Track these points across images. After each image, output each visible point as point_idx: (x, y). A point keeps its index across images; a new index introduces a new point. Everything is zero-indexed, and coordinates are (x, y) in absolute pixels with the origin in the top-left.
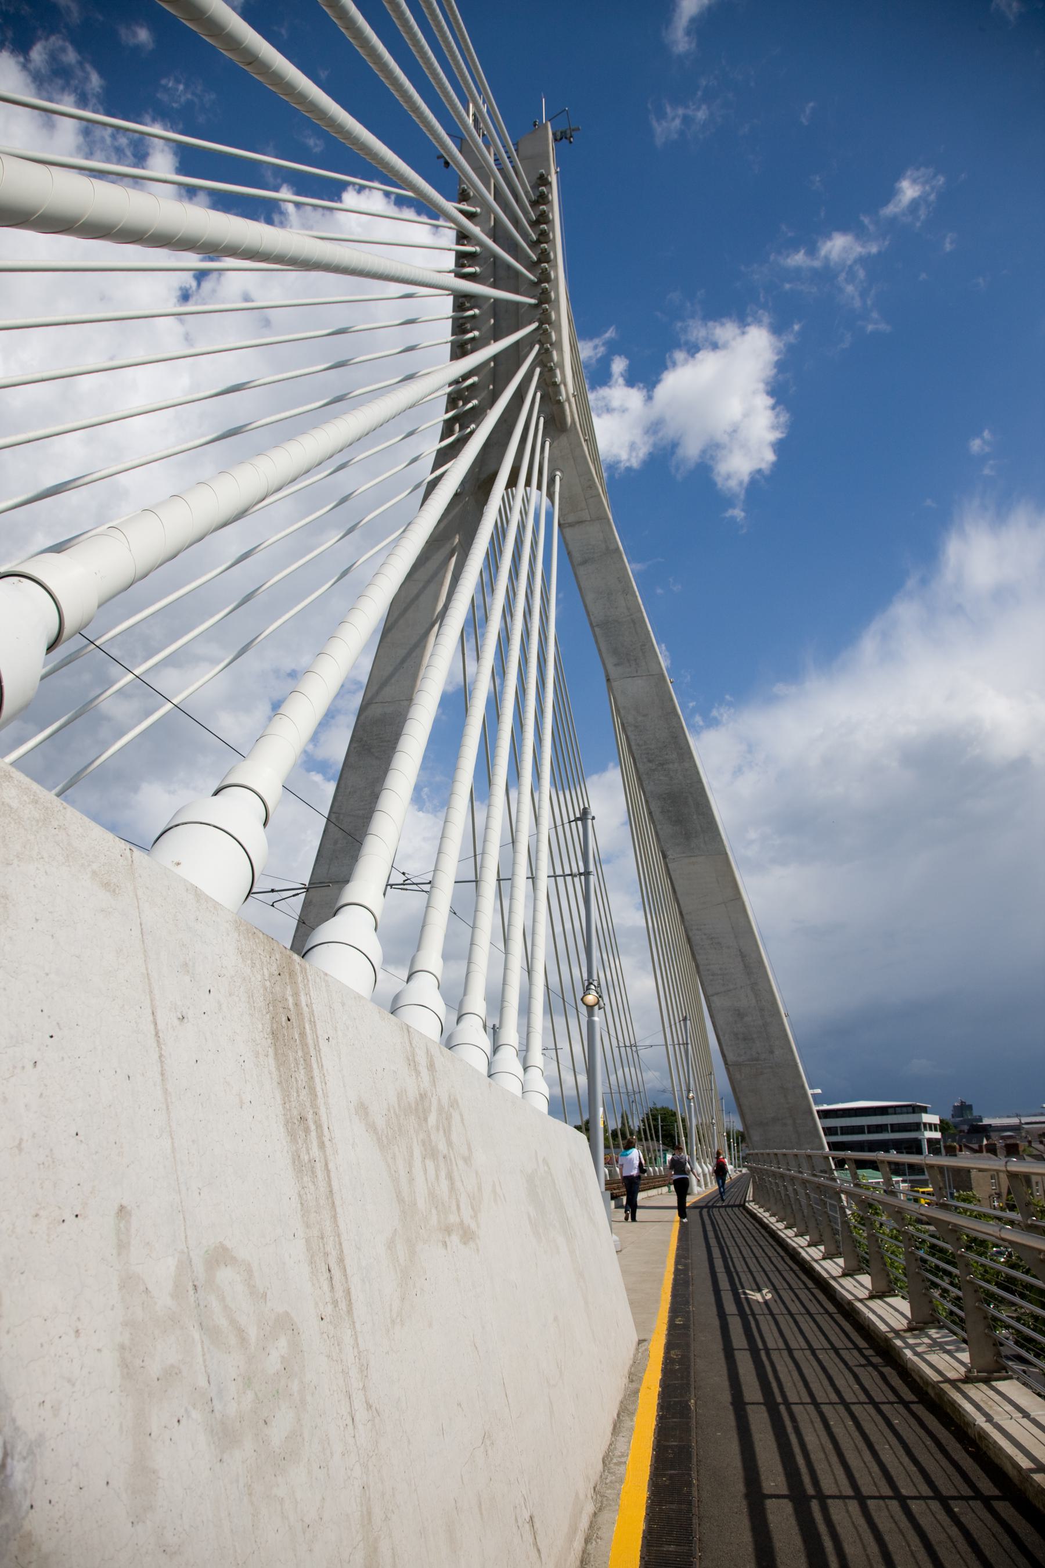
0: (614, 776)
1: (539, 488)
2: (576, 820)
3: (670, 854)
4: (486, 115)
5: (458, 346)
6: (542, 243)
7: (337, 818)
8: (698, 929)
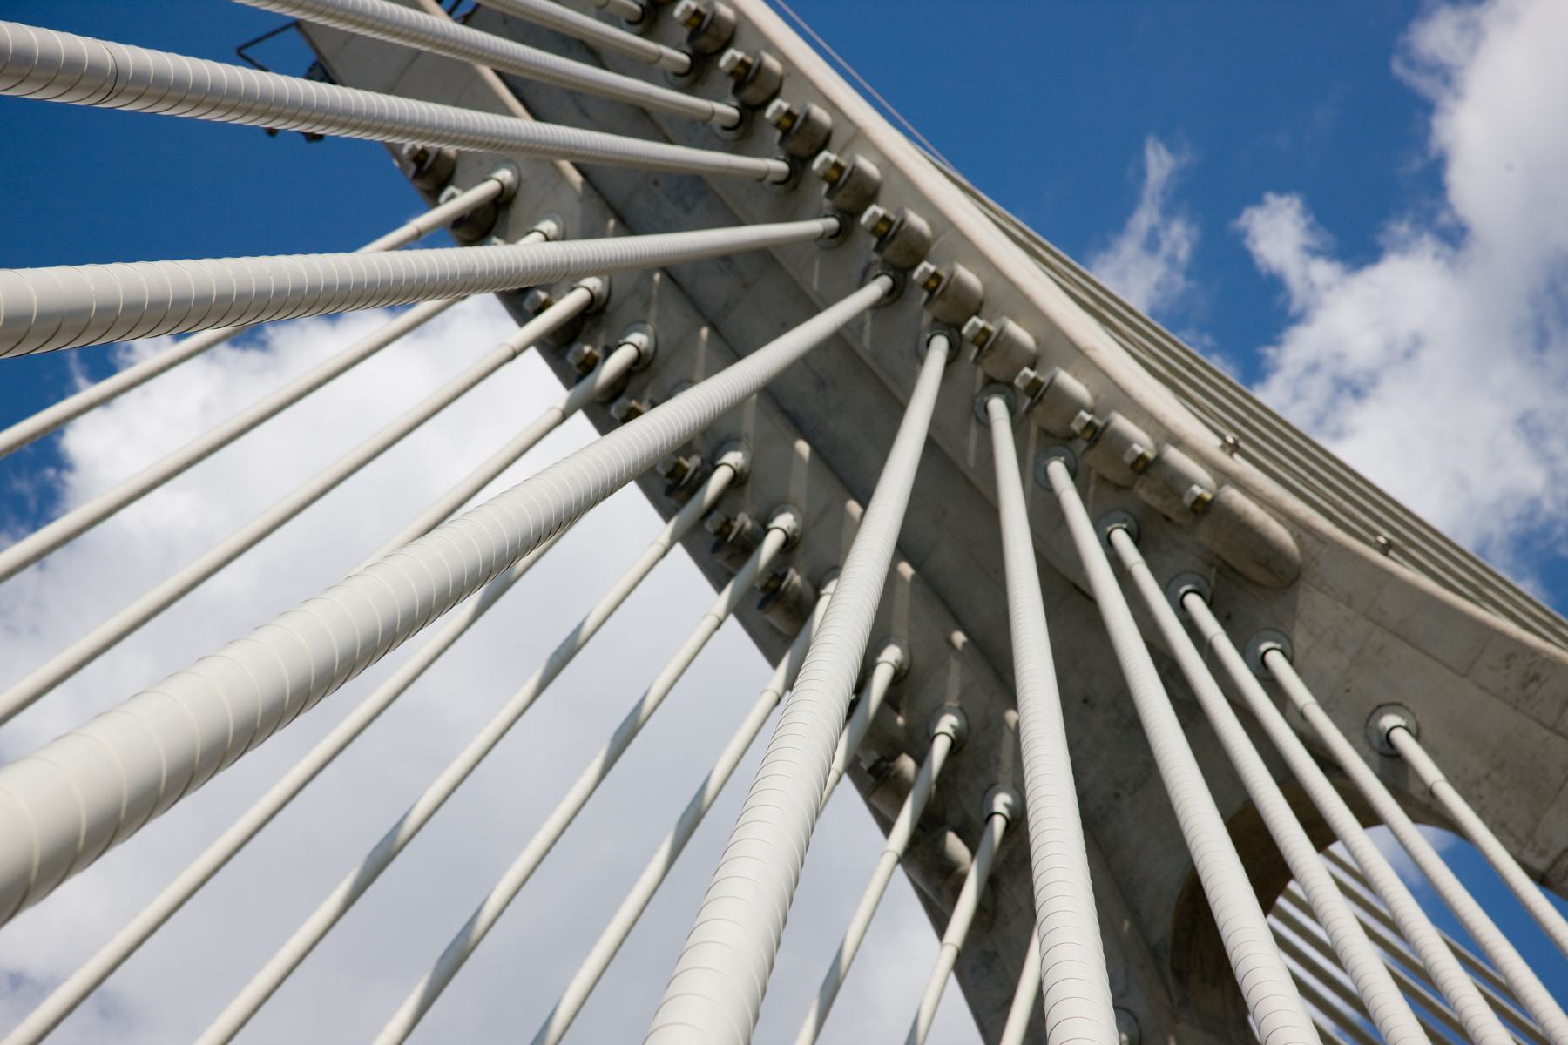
1: (1368, 816)
5: (762, 605)
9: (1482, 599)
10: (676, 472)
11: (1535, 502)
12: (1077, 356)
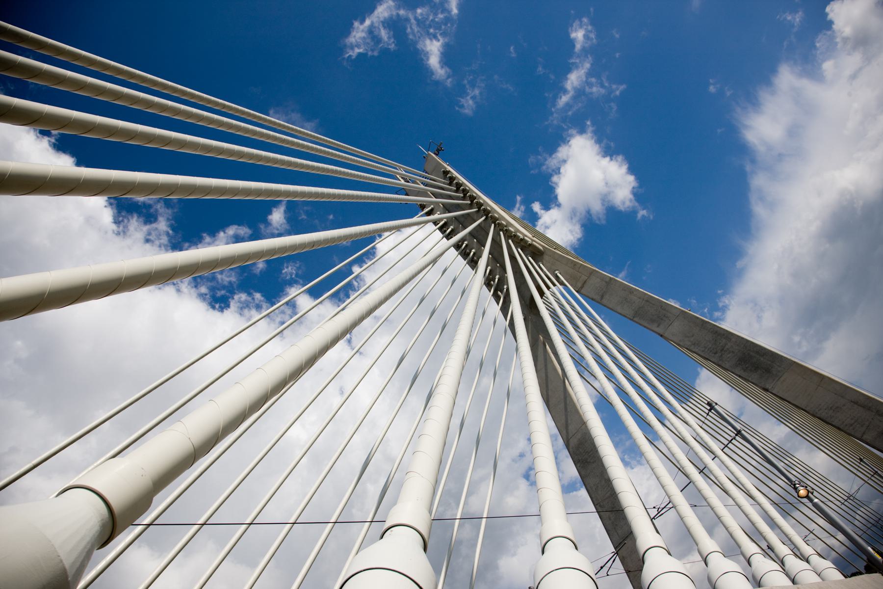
0: (705, 373)
1: (554, 285)
2: (710, 410)
3: (767, 387)
4: (406, 173)
5: (471, 262)
6: (460, 188)
7: (600, 506)
8: (819, 411)
10: (458, 245)
11: (572, 241)
12: (512, 225)
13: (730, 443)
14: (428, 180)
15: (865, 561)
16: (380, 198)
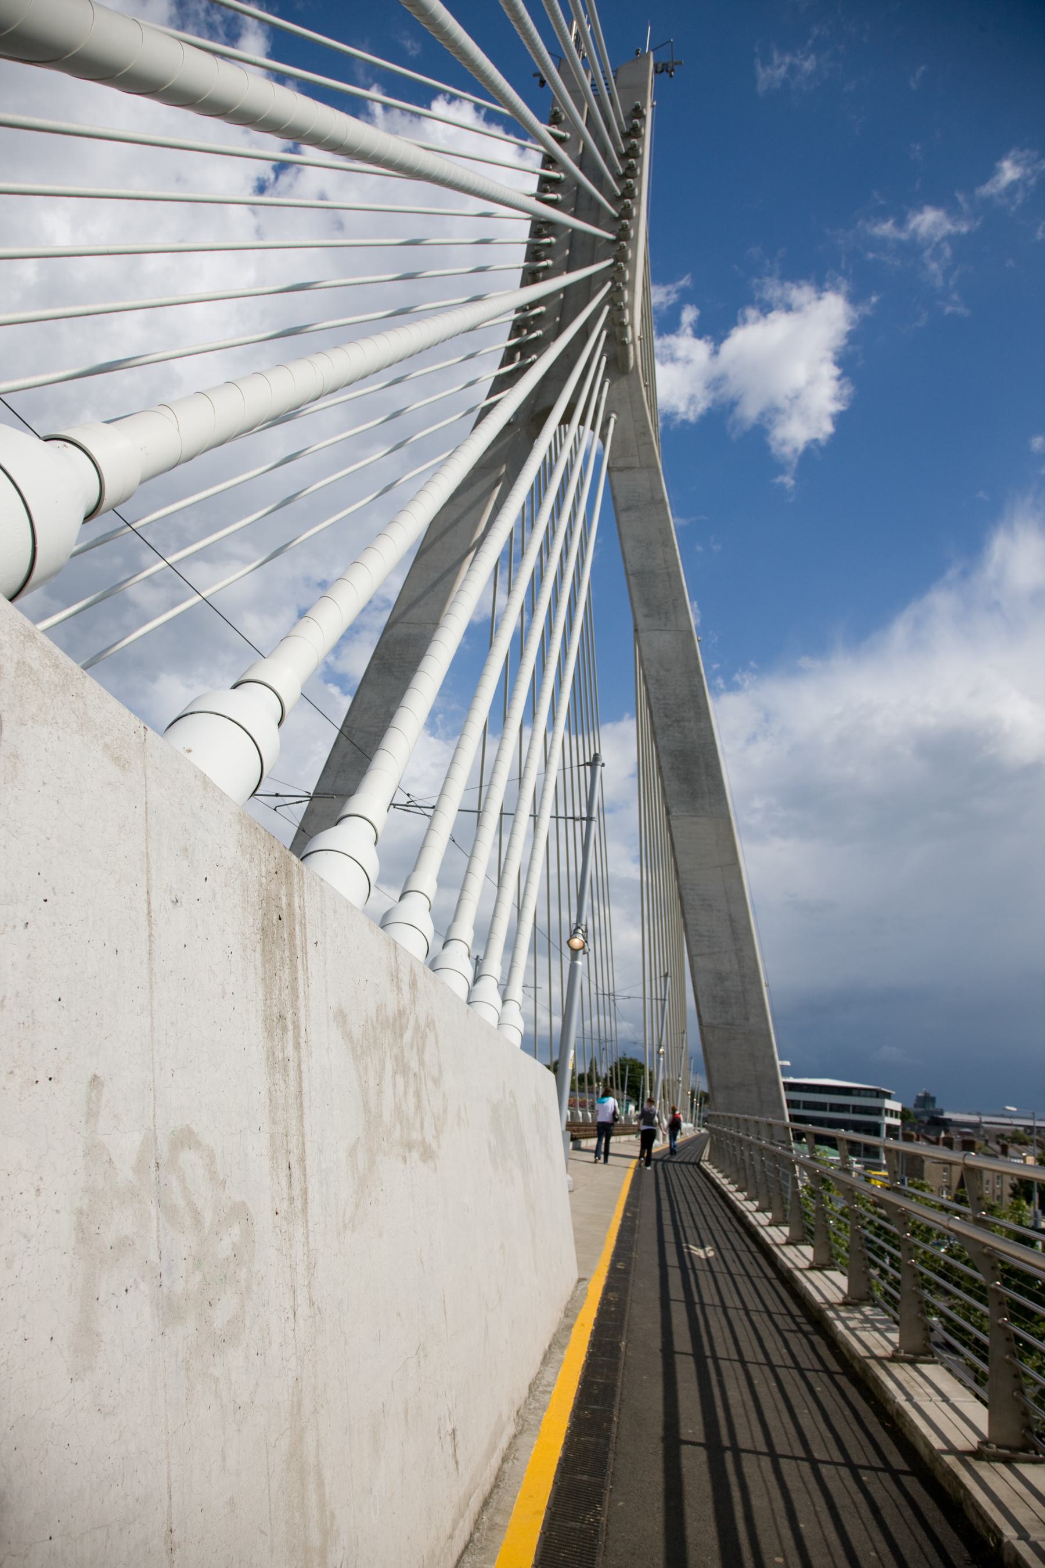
1: (593, 428)
3: (673, 810)
5: (530, 273)
8: (691, 889)
9: (650, 409)
11: (676, 414)
13: (564, 820)
14: (606, 92)
15: (551, 1060)
16: (519, 19)
